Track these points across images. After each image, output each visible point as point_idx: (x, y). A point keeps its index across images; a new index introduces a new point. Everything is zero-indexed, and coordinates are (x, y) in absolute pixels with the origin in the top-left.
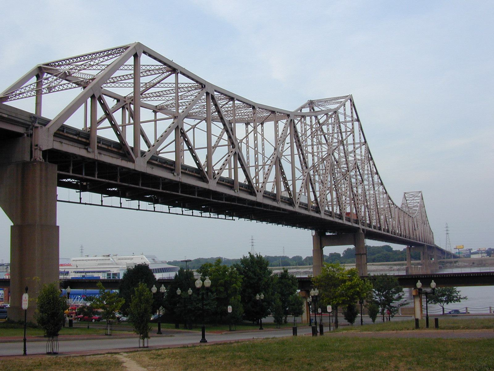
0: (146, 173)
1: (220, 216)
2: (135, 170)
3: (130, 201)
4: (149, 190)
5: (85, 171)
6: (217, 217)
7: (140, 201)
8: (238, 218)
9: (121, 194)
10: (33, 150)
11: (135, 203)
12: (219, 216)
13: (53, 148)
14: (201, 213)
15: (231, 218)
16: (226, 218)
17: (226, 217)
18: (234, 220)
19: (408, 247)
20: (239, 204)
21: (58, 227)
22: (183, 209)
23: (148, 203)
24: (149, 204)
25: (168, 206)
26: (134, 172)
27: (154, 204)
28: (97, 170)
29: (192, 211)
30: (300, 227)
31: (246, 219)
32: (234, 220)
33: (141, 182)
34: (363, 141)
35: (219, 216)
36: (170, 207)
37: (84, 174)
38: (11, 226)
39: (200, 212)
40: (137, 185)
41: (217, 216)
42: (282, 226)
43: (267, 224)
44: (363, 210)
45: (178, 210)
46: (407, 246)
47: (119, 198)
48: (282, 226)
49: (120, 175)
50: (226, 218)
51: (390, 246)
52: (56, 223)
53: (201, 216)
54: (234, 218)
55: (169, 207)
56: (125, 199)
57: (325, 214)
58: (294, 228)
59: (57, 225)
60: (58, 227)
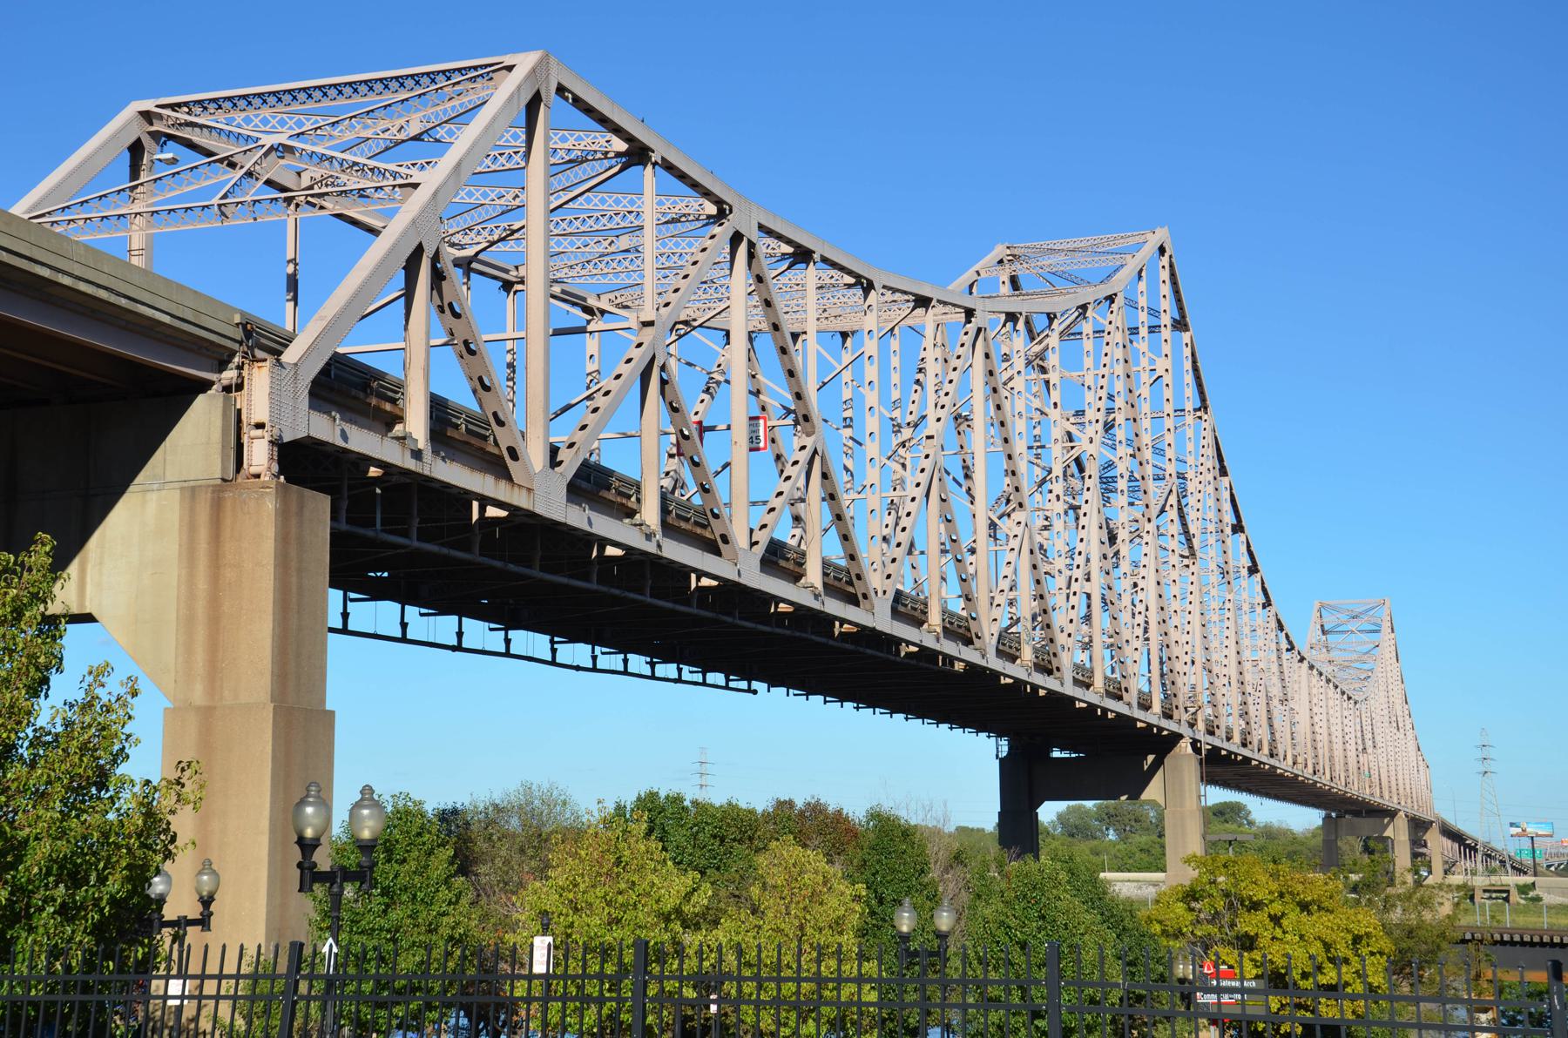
0: (565, 524)
1: (712, 677)
2: (874, 629)
3: (433, 617)
4: (744, 627)
5: (382, 513)
6: (701, 680)
7: (464, 619)
8: (766, 685)
9: (403, 592)
10: (245, 440)
11: (444, 627)
12: (708, 675)
13: (309, 437)
14: (652, 665)
15: (743, 685)
16: (732, 684)
17: (728, 680)
18: (755, 692)
19: (1327, 818)
20: (813, 637)
21: (332, 713)
22: (598, 649)
23: (487, 624)
24: (491, 630)
25: (547, 638)
26: (403, 480)
27: (506, 631)
28: (415, 512)
29: (622, 656)
30: (963, 726)
31: (791, 691)
32: (755, 692)
33: (416, 523)
34: (1229, 518)
35: (708, 675)
36: (556, 639)
37: (648, 595)
38: (166, 709)
39: (648, 659)
40: (641, 594)
41: (700, 675)
42: (907, 719)
43: (858, 708)
44: (167, 946)
45: (578, 652)
46: (1323, 813)
47: (456, 618)
48: (907, 719)
49: (350, 488)
50: (732, 684)
51: (1250, 807)
52: (323, 701)
53: (649, 674)
54: (755, 685)
55: (552, 642)
56: (416, 610)
57: (1103, 443)
58: (944, 727)
59: (328, 707)
60: (332, 713)
